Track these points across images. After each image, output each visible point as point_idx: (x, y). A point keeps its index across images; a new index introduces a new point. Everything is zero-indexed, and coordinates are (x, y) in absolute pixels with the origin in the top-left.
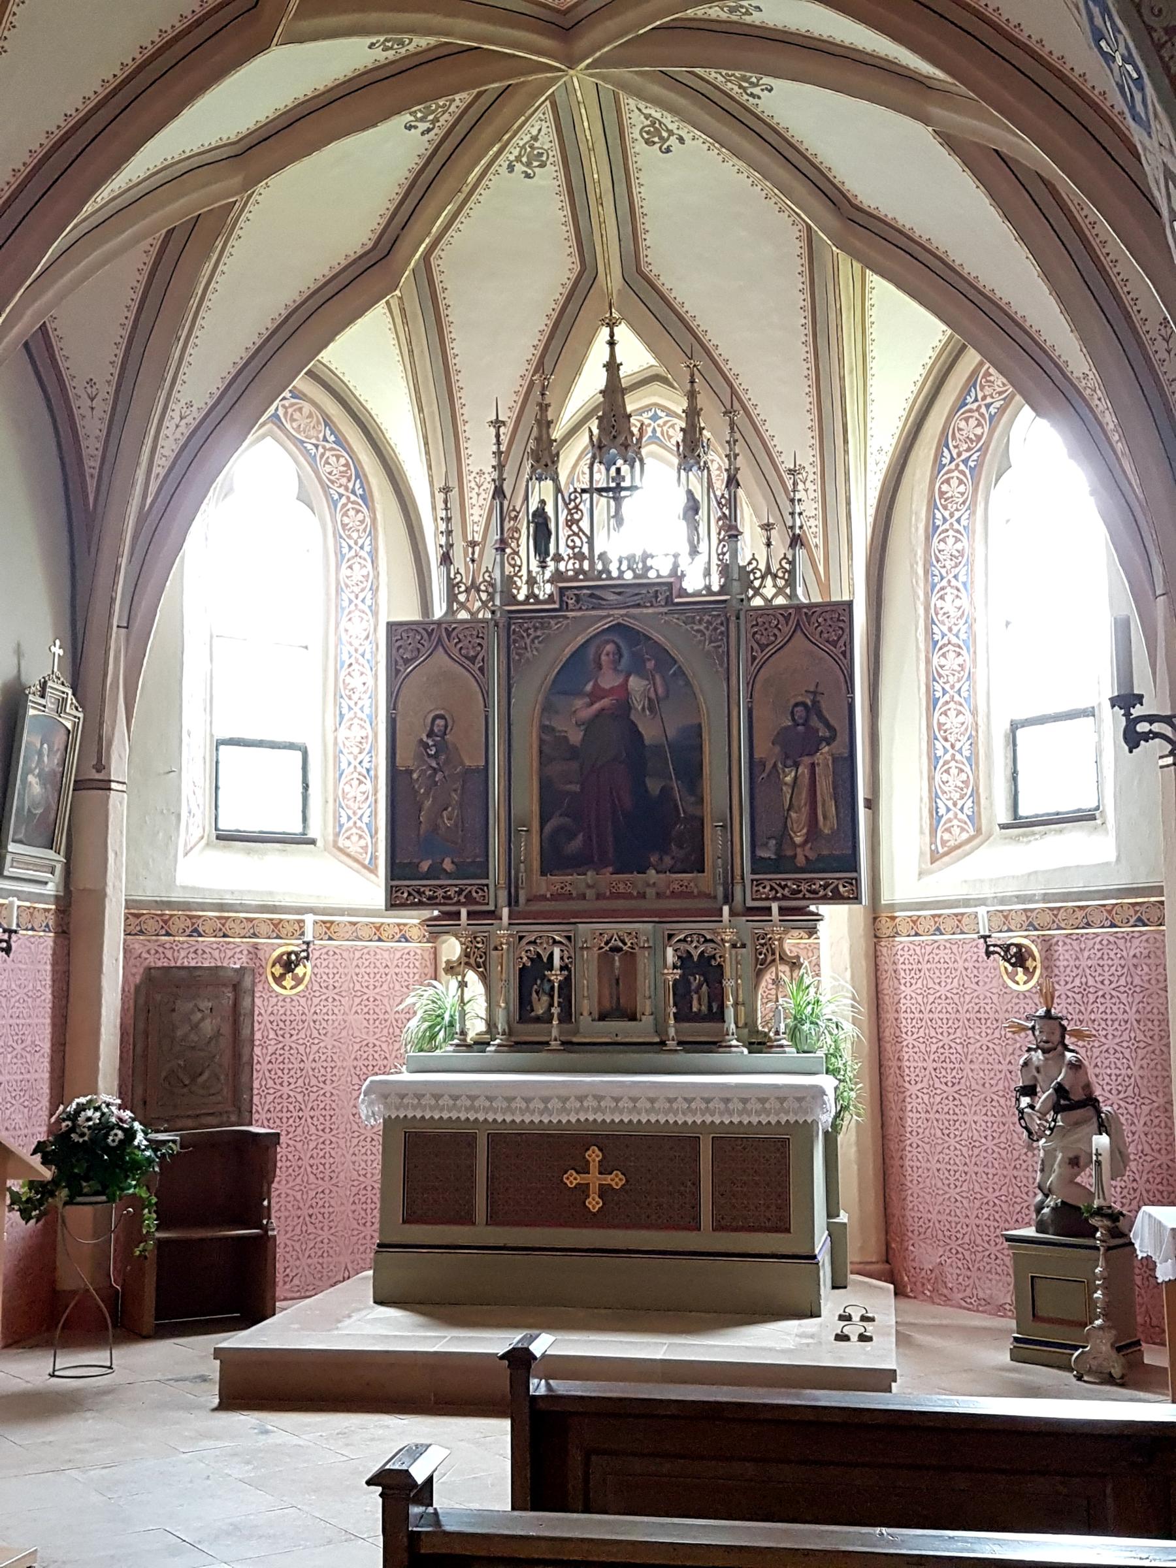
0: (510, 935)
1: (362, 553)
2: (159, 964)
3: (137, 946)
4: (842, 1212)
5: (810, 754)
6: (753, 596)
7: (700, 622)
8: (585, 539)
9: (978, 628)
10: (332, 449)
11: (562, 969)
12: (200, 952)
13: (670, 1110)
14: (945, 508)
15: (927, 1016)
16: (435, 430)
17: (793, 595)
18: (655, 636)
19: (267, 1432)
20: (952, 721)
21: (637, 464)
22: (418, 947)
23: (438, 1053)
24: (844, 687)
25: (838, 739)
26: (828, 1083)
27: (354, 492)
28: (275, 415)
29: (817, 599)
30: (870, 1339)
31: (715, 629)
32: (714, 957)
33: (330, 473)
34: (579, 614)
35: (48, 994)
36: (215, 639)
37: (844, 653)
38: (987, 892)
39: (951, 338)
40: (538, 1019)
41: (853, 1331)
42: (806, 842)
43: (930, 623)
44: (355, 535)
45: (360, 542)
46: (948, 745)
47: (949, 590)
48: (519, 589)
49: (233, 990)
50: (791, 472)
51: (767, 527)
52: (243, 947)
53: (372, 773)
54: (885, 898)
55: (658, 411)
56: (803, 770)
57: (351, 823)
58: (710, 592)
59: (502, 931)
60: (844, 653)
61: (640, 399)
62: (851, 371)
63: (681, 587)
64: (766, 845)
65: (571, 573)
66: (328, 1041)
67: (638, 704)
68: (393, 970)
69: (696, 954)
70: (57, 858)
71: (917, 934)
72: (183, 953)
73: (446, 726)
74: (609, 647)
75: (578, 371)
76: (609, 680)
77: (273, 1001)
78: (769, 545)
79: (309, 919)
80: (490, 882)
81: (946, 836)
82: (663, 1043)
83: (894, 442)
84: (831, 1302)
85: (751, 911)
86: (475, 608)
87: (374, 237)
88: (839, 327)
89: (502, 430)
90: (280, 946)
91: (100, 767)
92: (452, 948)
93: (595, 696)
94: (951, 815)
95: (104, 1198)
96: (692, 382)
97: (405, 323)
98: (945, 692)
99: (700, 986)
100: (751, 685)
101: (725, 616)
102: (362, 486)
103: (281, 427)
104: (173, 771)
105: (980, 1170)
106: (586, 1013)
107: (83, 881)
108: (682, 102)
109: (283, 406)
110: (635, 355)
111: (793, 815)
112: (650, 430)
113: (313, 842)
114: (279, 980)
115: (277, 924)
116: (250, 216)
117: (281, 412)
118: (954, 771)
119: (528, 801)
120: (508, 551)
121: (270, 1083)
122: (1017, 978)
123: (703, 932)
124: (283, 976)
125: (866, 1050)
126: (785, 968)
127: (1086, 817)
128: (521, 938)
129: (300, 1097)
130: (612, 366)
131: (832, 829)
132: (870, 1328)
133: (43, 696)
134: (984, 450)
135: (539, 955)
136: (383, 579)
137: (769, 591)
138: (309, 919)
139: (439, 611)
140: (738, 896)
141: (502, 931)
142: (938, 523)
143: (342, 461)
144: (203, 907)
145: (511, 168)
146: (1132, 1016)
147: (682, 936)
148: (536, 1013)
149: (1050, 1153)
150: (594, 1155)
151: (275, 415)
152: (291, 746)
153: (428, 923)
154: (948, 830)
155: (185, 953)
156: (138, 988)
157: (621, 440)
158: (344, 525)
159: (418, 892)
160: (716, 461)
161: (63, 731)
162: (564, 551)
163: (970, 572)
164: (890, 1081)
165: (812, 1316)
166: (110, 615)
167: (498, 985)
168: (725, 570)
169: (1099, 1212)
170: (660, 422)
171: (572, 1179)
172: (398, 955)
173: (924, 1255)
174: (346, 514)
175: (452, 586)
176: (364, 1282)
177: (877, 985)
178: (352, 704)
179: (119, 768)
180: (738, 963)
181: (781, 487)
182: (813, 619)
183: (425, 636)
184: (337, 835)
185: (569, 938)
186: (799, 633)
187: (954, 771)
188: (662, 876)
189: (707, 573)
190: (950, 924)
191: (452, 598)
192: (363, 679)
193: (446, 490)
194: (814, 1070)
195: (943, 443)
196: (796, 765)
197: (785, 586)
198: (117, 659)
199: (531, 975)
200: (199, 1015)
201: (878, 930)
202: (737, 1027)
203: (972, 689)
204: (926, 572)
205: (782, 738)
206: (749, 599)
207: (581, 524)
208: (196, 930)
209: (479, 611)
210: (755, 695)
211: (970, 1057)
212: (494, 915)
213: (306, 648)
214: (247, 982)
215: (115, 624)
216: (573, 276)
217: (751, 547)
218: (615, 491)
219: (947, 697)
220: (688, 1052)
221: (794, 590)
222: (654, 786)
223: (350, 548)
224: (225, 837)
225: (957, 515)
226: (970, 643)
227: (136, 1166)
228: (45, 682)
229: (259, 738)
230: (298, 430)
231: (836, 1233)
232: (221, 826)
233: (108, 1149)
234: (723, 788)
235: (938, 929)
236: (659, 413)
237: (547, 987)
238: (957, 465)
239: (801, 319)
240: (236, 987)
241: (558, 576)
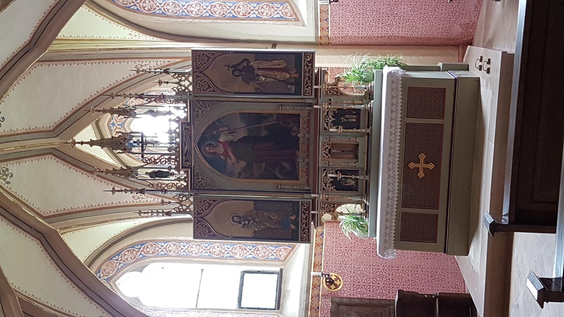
0: (322, 193)
1: (165, 246)
4: (438, 65)
5: (254, 70)
6: (188, 89)
7: (198, 112)
8: (163, 157)
10: (121, 257)
11: (337, 174)
13: (395, 134)
14: (155, 9)
15: (361, 26)
16: (115, 216)
17: (189, 74)
18: (203, 129)
19: (518, 305)
21: (132, 134)
22: (325, 229)
23: (369, 225)
24: (227, 55)
25: (248, 58)
26: (386, 70)
27: (139, 249)
28: (107, 280)
29: (190, 62)
30: (489, 60)
31: (201, 106)
32: (334, 112)
33: (131, 258)
34: (193, 161)
36: (198, 307)
37: (213, 54)
39: (86, 5)
40: (357, 183)
41: (486, 66)
42: (290, 73)
43: (201, 17)
44: (157, 249)
45: (160, 247)
46: (252, 12)
47: (188, 9)
48: (182, 185)
50: (138, 71)
51: (160, 83)
52: (323, 300)
53: (254, 245)
54: (313, 40)
55: (111, 126)
56: (260, 72)
57: (275, 254)
58: (186, 107)
59: (320, 197)
60: (213, 54)
61: (106, 130)
62: (97, 46)
63: (184, 119)
64: (290, 89)
65: (176, 163)
66: (362, 267)
68: (335, 240)
69: (333, 119)
71: (328, 28)
73: (236, 216)
74: (207, 149)
75: (93, 157)
76: (220, 150)
77: (345, 289)
78: (167, 83)
79: (312, 273)
80: (300, 201)
81: (289, 15)
82: (368, 134)
83: (127, 28)
84: (474, 73)
86: (189, 202)
87: (35, 239)
88: (79, 50)
89: (116, 189)
90: (323, 285)
92: (327, 217)
93: (226, 154)
94: (280, 12)
96: (99, 111)
97: (71, 227)
98: (230, 13)
99: (346, 118)
100: (225, 92)
102: (137, 245)
103: (111, 278)
105: (423, 7)
106: (355, 165)
109: (103, 277)
110: (88, 133)
111: (278, 77)
112: (118, 127)
113: (281, 270)
114: (337, 286)
117: (105, 278)
118: (262, 10)
119: (269, 184)
120: (166, 188)
121: (378, 291)
123: (324, 115)
124: (335, 285)
125: (374, 51)
126: (340, 84)
128: (324, 189)
129: (384, 279)
130: (92, 143)
131: (284, 62)
132: (485, 59)
135: (330, 182)
136: (174, 238)
137: (186, 83)
138: (312, 273)
139: (188, 216)
140: (311, 101)
141: (320, 197)
142: (161, 12)
143: (126, 253)
145: (8, 183)
147: (325, 125)
148: (354, 184)
151: (107, 280)
152: (242, 278)
153: (316, 226)
154: (286, 14)
157: (122, 141)
158: (153, 253)
159: (304, 230)
160: (132, 102)
162: (167, 165)
164: (386, 41)
165: (479, 81)
167: (342, 200)
168: (177, 101)
170: (115, 122)
171: (421, 174)
172: (328, 237)
173: (456, 31)
174: (148, 252)
175: (179, 212)
176: (460, 259)
177: (348, 45)
178: (226, 252)
180: (337, 102)
181: (143, 76)
182: (198, 66)
183: (200, 223)
184: (279, 260)
185: (324, 170)
186: (204, 72)
187: (262, 10)
188: (301, 131)
189: (178, 108)
190: (324, 15)
191: (184, 212)
192: (216, 247)
193: (140, 213)
194: (381, 74)
195: (128, 9)
196: (258, 75)
197: (185, 77)
199: (339, 186)
201: (325, 43)
202: (362, 104)
204: (181, 18)
205: (247, 81)
206: (189, 91)
207: (156, 158)
209: (190, 201)
210: (228, 91)
211: (378, 10)
212: (314, 200)
213: (202, 270)
214: (337, 300)
216: (54, 157)
217: (168, 90)
218: (143, 143)
219: (232, 12)
220: (372, 125)
221: (186, 73)
222: (264, 133)
223: (162, 251)
224: (279, 305)
225: (158, 4)
229: (238, 290)
230: (113, 271)
231: (447, 68)
232: (274, 307)
234: (267, 105)
235: (326, 20)
236: (111, 122)
237: (344, 180)
238: (138, 3)
239: (75, 66)
240: (339, 304)
241: (177, 169)
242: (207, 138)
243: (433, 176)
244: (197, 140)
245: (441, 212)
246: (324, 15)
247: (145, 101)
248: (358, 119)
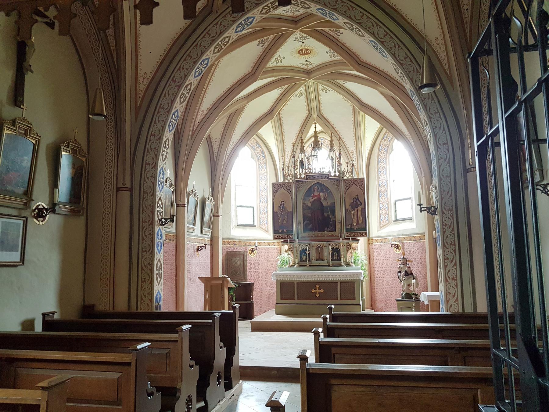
9: (388, 182)
17: (352, 176)
18: (326, 185)
20: (383, 200)
26: (362, 272)
38: (391, 234)
40: (304, 261)
49: (243, 256)
51: (347, 163)
55: (324, 139)
59: (296, 244)
67: (322, 198)
76: (316, 193)
77: (250, 258)
79: (256, 242)
85: (345, 239)
86: (290, 180)
88: (360, 124)
91: (217, 213)
92: (286, 247)
93: (314, 196)
100: (345, 194)
101: (338, 180)
108: (330, 85)
110: (319, 128)
114: (250, 254)
115: (250, 243)
119: (300, 218)
127: (410, 219)
134: (388, 147)
137: (348, 176)
138: (256, 242)
141: (296, 244)
144: (236, 239)
146: (419, 257)
148: (304, 260)
149: (404, 284)
150: (317, 286)
152: (251, 207)
155: (233, 248)
162: (307, 168)
163: (386, 171)
168: (339, 172)
169: (414, 294)
171: (313, 291)
179: (221, 213)
181: (350, 156)
191: (284, 177)
201: (369, 243)
203: (387, 194)
205: (351, 205)
217: (344, 167)
222: (326, 214)
224: (239, 226)
226: (387, 185)
231: (363, 301)
234: (340, 215)
241: (306, 173)
242: (322, 187)
243: (314, 297)
244: (320, 182)
245: (296, 301)
246: (267, 244)
247: (338, 156)
248: (335, 260)
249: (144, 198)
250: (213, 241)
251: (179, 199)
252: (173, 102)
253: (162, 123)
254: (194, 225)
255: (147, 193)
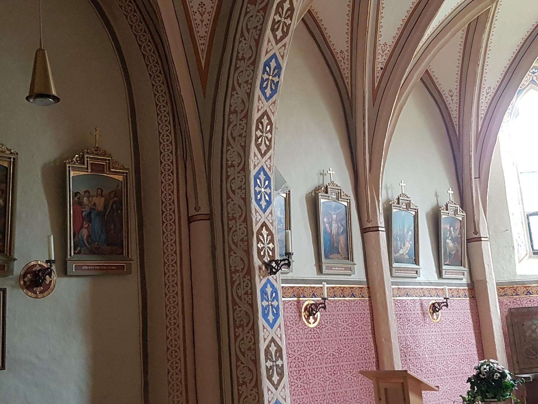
2: (515, 307)
3: (505, 300)
12: (532, 301)
35: (471, 321)
70: (466, 269)
72: (525, 302)
91: (476, 232)
95: (496, 400)
104: (508, 229)
107: (477, 276)
116: (499, 11)
122: (310, 321)
133: (447, 210)
155: (525, 302)
156: (507, 317)
161: (459, 221)
166: (471, 175)
179: (483, 232)
198: (476, 191)
200: (535, 326)
208: (528, 292)
215: (473, 177)
227: (507, 387)
228: (447, 204)
233: (494, 380)
249: (230, 229)
250: (475, 291)
251: (365, 218)
252: (258, 42)
253: (245, 87)
254: (416, 261)
255: (234, 218)
